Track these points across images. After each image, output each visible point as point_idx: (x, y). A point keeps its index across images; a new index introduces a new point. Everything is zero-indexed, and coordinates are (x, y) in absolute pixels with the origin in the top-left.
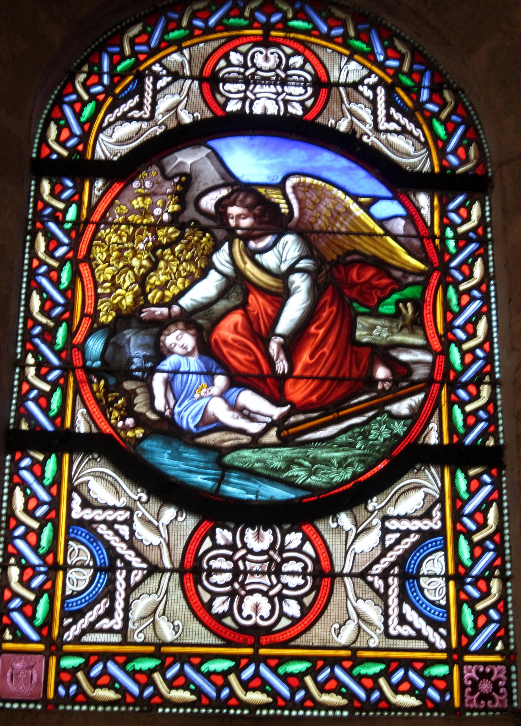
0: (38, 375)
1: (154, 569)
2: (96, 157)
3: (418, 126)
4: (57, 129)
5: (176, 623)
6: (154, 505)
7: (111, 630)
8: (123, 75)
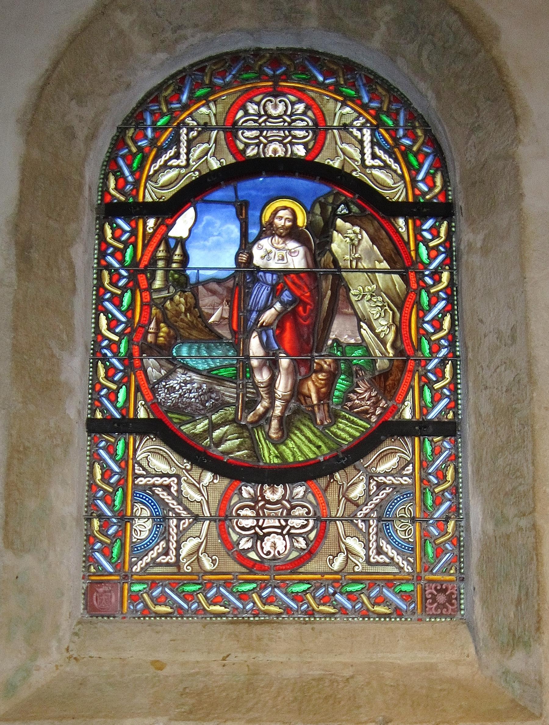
0: (109, 329)
1: (197, 518)
2: (146, 200)
3: (396, 161)
4: (115, 179)
5: (214, 558)
6: (196, 472)
7: (168, 564)
8: (164, 129)
